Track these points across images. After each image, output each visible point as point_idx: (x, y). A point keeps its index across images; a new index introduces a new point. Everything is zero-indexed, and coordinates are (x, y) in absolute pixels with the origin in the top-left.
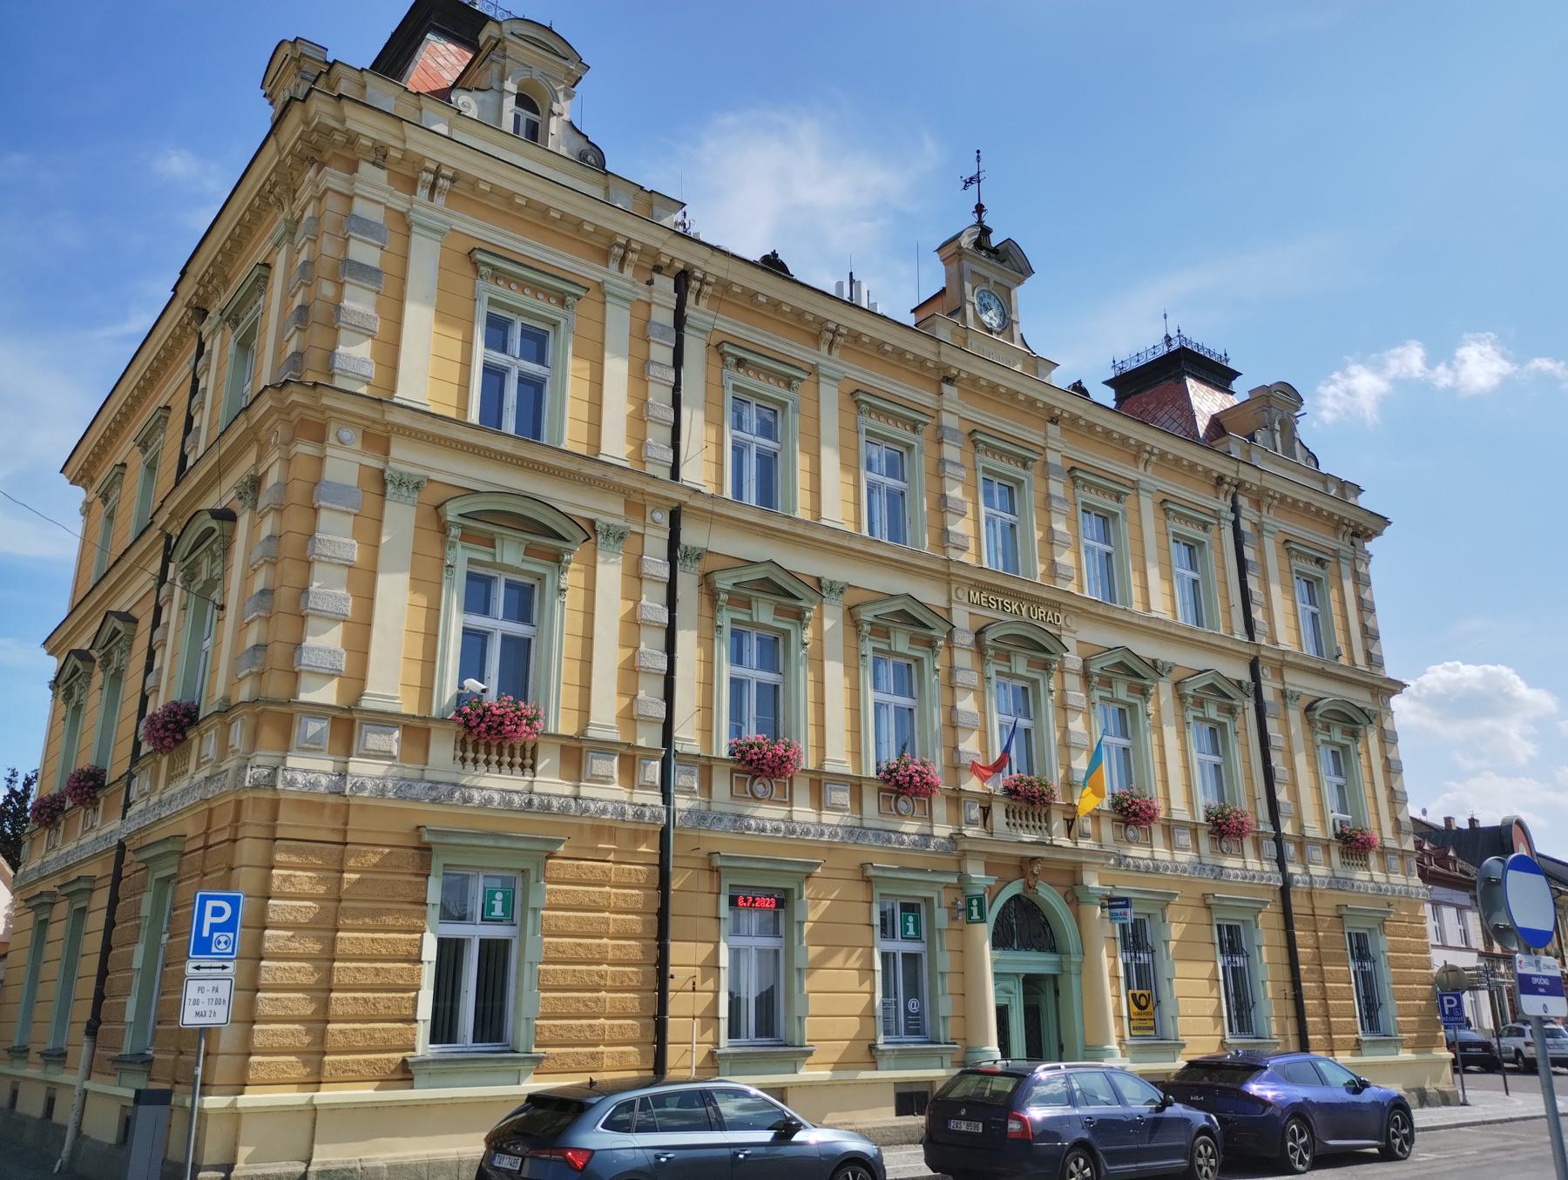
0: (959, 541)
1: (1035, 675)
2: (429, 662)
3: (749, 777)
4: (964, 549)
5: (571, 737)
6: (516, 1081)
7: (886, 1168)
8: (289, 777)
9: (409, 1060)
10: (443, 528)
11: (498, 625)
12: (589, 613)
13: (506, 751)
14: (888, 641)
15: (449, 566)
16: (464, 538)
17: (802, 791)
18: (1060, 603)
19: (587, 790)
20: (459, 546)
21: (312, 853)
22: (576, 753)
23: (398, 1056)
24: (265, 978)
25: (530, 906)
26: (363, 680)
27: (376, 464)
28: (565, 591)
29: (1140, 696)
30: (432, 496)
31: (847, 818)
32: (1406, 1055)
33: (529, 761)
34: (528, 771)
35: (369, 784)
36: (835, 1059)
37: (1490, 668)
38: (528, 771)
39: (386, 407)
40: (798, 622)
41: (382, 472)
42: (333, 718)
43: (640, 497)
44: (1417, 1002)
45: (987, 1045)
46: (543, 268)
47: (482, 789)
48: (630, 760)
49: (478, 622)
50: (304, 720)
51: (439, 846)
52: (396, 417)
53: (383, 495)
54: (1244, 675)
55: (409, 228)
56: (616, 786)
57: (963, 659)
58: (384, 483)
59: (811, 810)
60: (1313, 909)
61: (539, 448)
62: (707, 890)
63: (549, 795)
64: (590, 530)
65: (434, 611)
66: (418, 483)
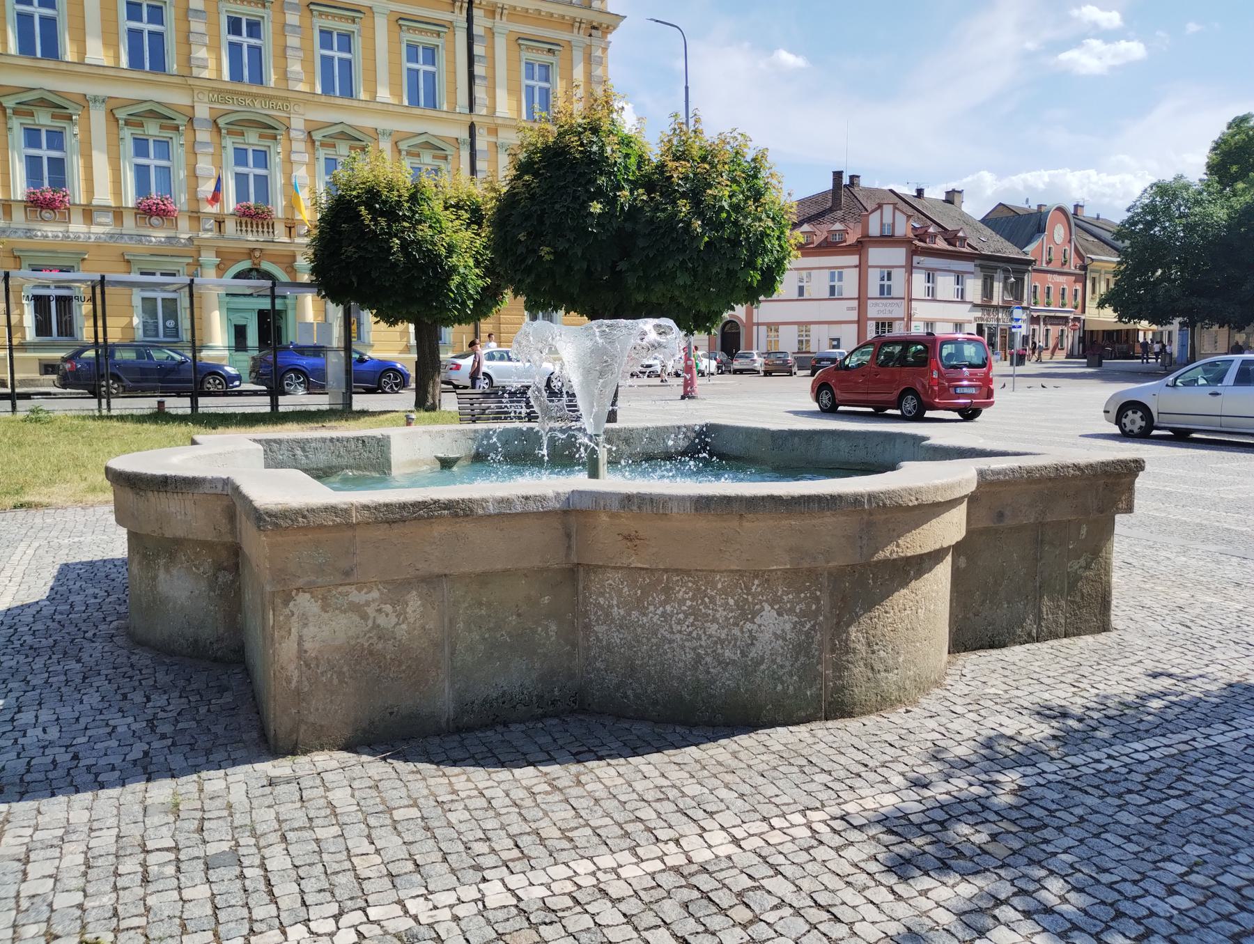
0: (199, 63)
1: (59, 124)
4: (205, 67)
10: (219, 130)
16: (228, 133)
17: (77, 216)
22: (89, 213)
27: (494, 140)
33: (271, 230)
35: (82, 236)
37: (1052, 172)
46: (348, 6)
52: (500, 121)
54: (465, 135)
55: (493, 34)
57: (299, 146)
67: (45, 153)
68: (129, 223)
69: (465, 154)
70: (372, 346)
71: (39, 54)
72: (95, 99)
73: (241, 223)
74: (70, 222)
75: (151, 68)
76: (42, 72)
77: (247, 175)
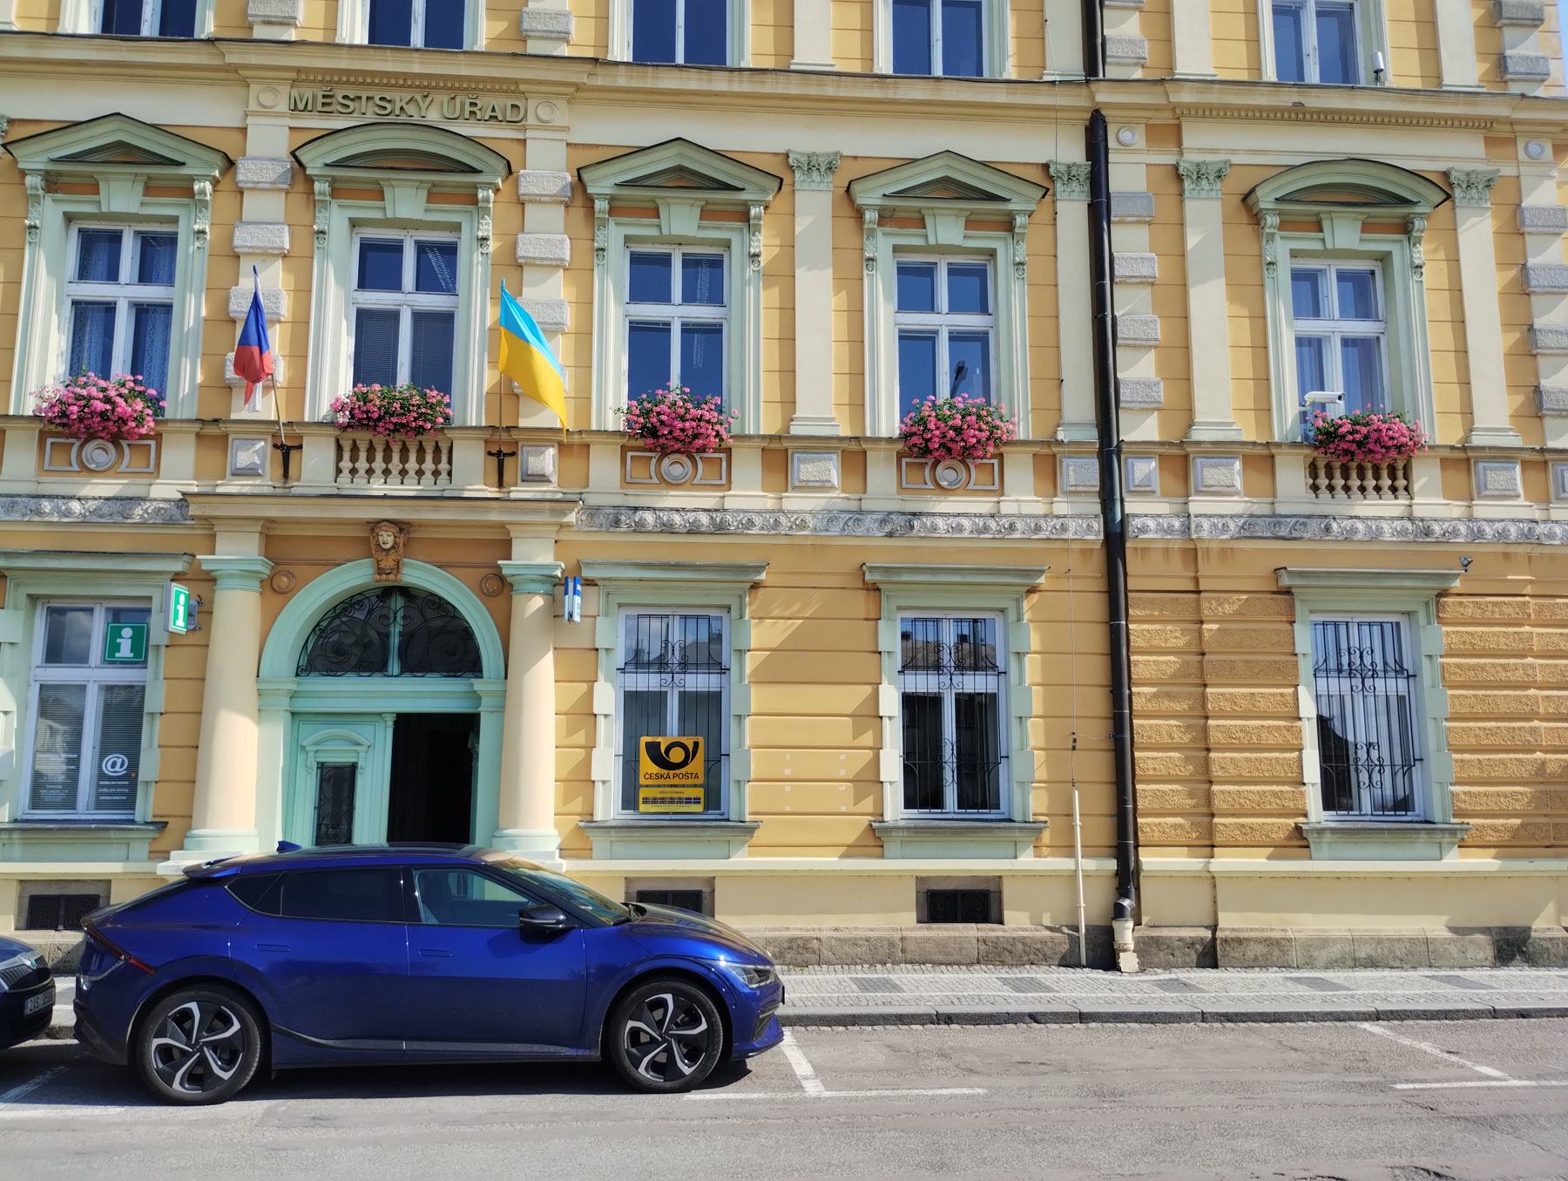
1: (163, 207)
2: (1263, 381)
3: (77, 444)
5: (1452, 448)
6: (1013, 854)
7: (72, 1007)
8: (929, 523)
9: (1304, 827)
10: (1256, 218)
11: (1335, 326)
12: (1456, 292)
13: (1385, 473)
14: (1320, 235)
15: (1270, 263)
16: (1283, 226)
17: (747, 467)
18: (516, 82)
19: (1483, 509)
20: (1277, 238)
21: (1152, 602)
23: (1291, 822)
24: (1215, 737)
25: (1424, 653)
26: (1190, 410)
28: (1421, 267)
29: (1003, 234)
30: (846, 173)
31: (836, 498)
32: (1483, 862)
33: (1401, 483)
34: (1401, 492)
35: (758, 520)
36: (851, 839)
38: (1401, 492)
39: (1169, 87)
40: (1403, 237)
41: (1176, 167)
42: (1161, 456)
43: (1508, 128)
44: (1539, 755)
45: (204, 826)
47: (86, 499)
48: (1048, 461)
49: (1311, 327)
50: (1130, 461)
51: (888, 586)
52: (1186, 96)
53: (1181, 194)
54: (1070, 151)
56: (1521, 501)
58: (1179, 178)
59: (1036, 498)
60: (1196, 579)
61: (461, 57)
62: (863, 617)
63: (1222, 516)
64: (1445, 187)
65: (1259, 319)
66: (1219, 171)
67: (943, 321)
68: (882, 476)
69: (1073, 212)
70: (750, 830)
71: (938, 69)
72: (810, 165)
73: (355, 449)
74: (157, 472)
75: (947, 68)
76: (688, 105)
77: (665, 328)
